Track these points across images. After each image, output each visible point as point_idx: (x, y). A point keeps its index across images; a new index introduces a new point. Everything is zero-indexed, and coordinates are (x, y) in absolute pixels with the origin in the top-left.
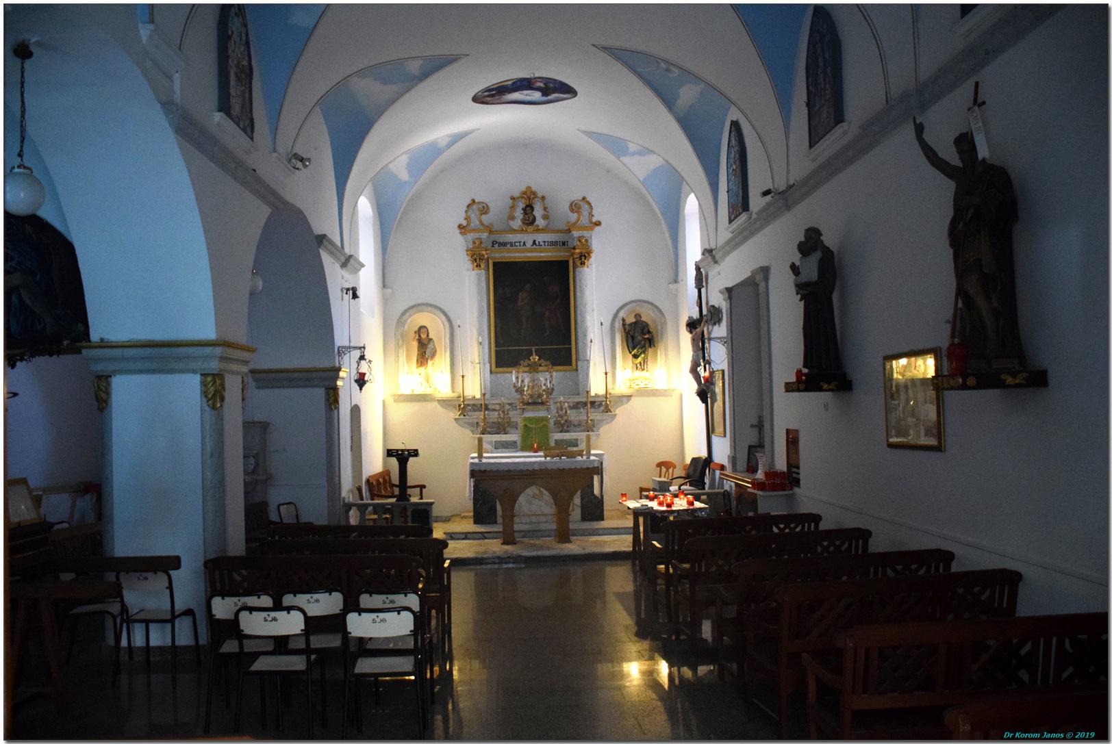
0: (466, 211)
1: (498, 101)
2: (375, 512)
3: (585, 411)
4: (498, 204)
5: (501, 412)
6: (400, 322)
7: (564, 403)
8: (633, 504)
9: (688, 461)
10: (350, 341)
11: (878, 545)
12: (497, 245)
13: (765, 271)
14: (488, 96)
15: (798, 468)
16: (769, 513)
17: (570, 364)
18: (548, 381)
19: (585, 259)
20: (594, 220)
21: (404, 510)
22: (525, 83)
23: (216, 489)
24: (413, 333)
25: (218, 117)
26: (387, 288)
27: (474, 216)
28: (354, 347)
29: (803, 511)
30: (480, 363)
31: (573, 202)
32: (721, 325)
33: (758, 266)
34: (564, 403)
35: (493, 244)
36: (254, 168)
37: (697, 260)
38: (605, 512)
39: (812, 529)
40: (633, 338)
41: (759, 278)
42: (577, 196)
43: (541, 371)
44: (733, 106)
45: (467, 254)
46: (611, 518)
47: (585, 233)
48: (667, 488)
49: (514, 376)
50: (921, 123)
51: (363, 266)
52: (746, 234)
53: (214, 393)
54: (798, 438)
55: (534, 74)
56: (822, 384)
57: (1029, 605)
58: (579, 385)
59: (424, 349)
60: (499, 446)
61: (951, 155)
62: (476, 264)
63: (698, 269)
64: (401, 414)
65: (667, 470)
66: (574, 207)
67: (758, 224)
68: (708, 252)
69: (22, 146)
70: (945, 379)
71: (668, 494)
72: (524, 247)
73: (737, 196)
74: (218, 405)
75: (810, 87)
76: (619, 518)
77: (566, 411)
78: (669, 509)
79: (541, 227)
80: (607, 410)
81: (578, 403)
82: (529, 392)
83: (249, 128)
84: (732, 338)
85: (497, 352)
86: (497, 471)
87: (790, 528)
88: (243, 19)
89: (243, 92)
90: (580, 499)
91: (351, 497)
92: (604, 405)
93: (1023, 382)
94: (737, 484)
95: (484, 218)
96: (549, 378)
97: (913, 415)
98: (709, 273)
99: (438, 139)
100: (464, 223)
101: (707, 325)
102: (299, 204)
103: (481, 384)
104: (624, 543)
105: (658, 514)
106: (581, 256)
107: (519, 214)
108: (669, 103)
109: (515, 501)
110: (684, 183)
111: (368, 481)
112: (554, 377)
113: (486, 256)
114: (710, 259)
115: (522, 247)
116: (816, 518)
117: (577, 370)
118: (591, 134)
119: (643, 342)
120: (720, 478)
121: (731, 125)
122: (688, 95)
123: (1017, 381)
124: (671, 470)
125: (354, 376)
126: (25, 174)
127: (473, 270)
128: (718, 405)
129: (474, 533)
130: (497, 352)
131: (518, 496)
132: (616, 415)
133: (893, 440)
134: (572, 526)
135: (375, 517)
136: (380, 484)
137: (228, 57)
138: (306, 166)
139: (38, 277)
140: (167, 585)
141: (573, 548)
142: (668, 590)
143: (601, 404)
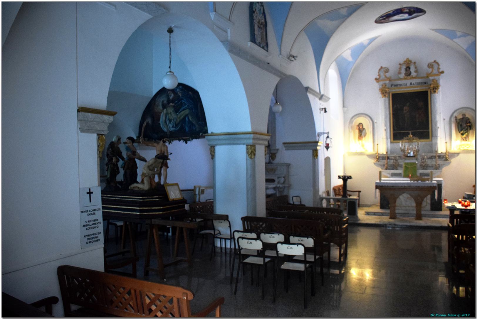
0: (379, 72)
6: (351, 122)
7: (425, 156)
14: (382, 20)
20: (440, 71)
22: (399, 11)
23: (252, 189)
25: (250, 44)
27: (382, 74)
34: (425, 156)
36: (268, 62)
40: (461, 125)
47: (436, 78)
49: (400, 145)
53: (251, 152)
55: (402, 6)
58: (432, 149)
60: (393, 175)
74: (253, 157)
79: (414, 76)
81: (432, 156)
83: (265, 46)
86: (388, 186)
89: (262, 33)
92: (445, 158)
100: (378, 77)
102: (295, 75)
107: (403, 71)
113: (388, 91)
119: (466, 128)
126: (172, 74)
127: (382, 97)
130: (428, 129)
132: (450, 162)
137: (254, 20)
138: (295, 59)
139: (194, 111)
140: (229, 225)
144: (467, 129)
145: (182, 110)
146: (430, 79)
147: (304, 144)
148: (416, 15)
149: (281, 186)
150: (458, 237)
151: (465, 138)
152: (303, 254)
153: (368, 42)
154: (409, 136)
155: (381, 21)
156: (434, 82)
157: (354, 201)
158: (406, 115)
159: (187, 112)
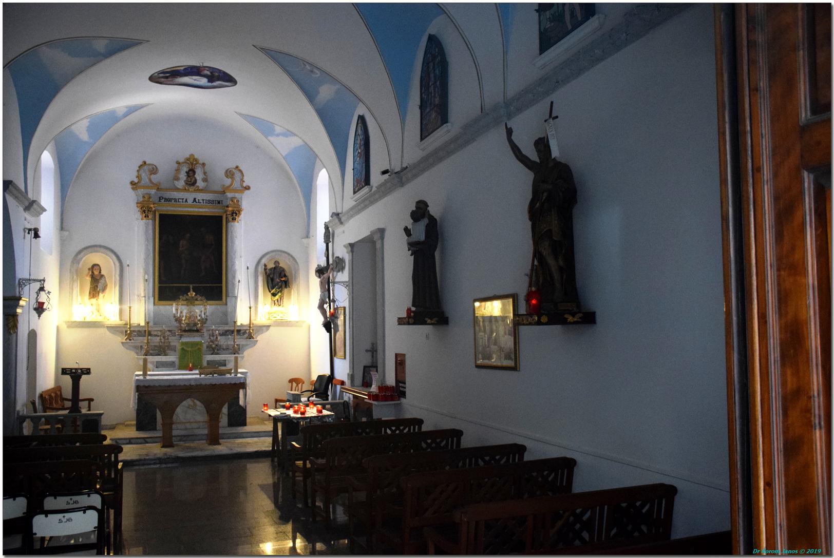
2: (47, 423)
3: (233, 337)
4: (166, 169)
5: (162, 338)
7: (216, 330)
8: (273, 413)
9: (314, 378)
10: (30, 275)
11: (467, 442)
12: (164, 200)
13: (382, 231)
14: (163, 77)
15: (405, 383)
16: (381, 419)
17: (220, 298)
19: (236, 216)
20: (245, 185)
21: (75, 420)
24: (87, 269)
26: (65, 231)
27: (145, 176)
29: (408, 416)
30: (145, 297)
31: (228, 169)
32: (344, 271)
33: (377, 228)
35: (160, 199)
37: (327, 221)
38: (247, 419)
39: (416, 430)
40: (272, 280)
41: (376, 237)
42: (231, 165)
43: (197, 305)
44: (361, 103)
45: (137, 206)
46: (252, 424)
47: (237, 195)
48: (299, 400)
50: (511, 128)
51: (45, 210)
52: (367, 202)
54: (405, 361)
55: (203, 63)
56: (426, 319)
57: (582, 483)
58: (228, 317)
59: (97, 283)
60: (159, 365)
61: (532, 154)
62: (144, 215)
63: (327, 228)
64: (72, 337)
65: (297, 385)
67: (377, 196)
68: (336, 215)
70: (524, 318)
71: (301, 404)
73: (361, 173)
75: (423, 95)
76: (258, 423)
77: (217, 338)
78: (303, 416)
79: (201, 188)
80: (250, 337)
82: (186, 321)
85: (221, 282)
90: (227, 409)
91: (25, 410)
92: (248, 334)
93: (579, 320)
94: (354, 396)
95: (153, 176)
96: (202, 310)
97: (495, 344)
98: (335, 231)
99: (117, 108)
100: (136, 180)
101: (332, 272)
103: (145, 315)
104: (265, 444)
105: (294, 420)
106: (233, 213)
107: (183, 176)
108: (310, 96)
109: (173, 411)
111: (41, 396)
112: (208, 310)
113: (154, 209)
114: (337, 220)
115: (184, 203)
116: (420, 422)
117: (226, 304)
118: (245, 116)
120: (341, 391)
121: (358, 117)
122: (326, 92)
123: (575, 320)
124: (300, 385)
125: (33, 304)
127: (142, 219)
128: (340, 335)
129: (137, 438)
130: (160, 288)
131: (177, 406)
132: (257, 341)
133: (480, 362)
134: (221, 431)
135: (48, 427)
136: (53, 398)
141: (222, 449)
142: (305, 481)
143: (245, 332)
144: (281, 287)
146: (226, 196)
148: (220, 84)
150: (305, 464)
152: (95, 528)
153: (126, 110)
155: (160, 79)
157: (96, 418)
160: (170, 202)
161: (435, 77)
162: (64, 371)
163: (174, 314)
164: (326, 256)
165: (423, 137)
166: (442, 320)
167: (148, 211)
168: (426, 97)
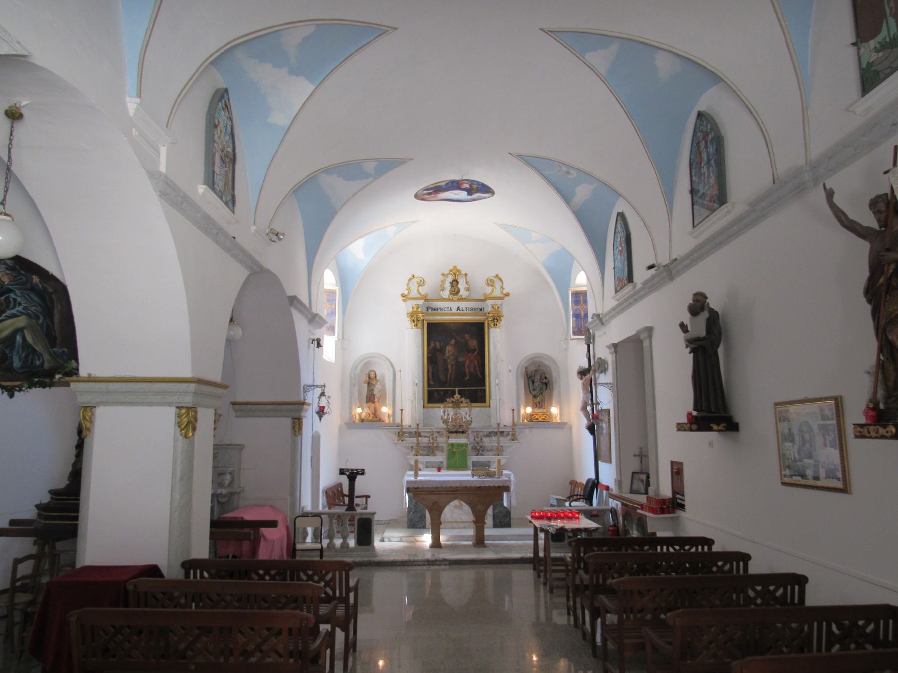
0: (408, 284)
1: (434, 199)
3: (496, 439)
11: (815, 597)
13: (649, 330)
15: (683, 495)
17: (484, 401)
18: (468, 415)
20: (505, 292)
22: (455, 184)
25: (202, 189)
28: (316, 386)
32: (606, 373)
41: (642, 336)
42: (492, 274)
43: (462, 407)
49: (439, 412)
52: (631, 300)
56: (712, 425)
66: (489, 282)
69: (5, 196)
72: (451, 312)
74: (190, 434)
77: (481, 439)
79: (464, 297)
81: (491, 432)
84: (617, 384)
87: (685, 550)
88: (229, 113)
96: (470, 413)
100: (406, 292)
106: (494, 319)
107: (448, 286)
108: (567, 199)
110: (575, 261)
113: (422, 318)
114: (598, 321)
117: (490, 406)
119: (541, 386)
122: (582, 193)
127: (412, 328)
130: (484, 385)
131: (444, 507)
139: (41, 321)
143: (509, 433)
145: (6, 316)
147: (276, 407)
149: (224, 491)
151: (539, 402)
154: (455, 396)
156: (495, 309)
158: (449, 361)
159: (22, 321)
160: (436, 312)
161: (708, 156)
162: (342, 472)
163: (442, 416)
164: (588, 357)
165: (696, 224)
166: (731, 426)
167: (417, 320)
168: (697, 180)
